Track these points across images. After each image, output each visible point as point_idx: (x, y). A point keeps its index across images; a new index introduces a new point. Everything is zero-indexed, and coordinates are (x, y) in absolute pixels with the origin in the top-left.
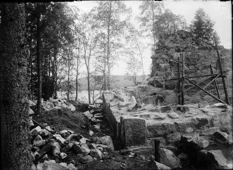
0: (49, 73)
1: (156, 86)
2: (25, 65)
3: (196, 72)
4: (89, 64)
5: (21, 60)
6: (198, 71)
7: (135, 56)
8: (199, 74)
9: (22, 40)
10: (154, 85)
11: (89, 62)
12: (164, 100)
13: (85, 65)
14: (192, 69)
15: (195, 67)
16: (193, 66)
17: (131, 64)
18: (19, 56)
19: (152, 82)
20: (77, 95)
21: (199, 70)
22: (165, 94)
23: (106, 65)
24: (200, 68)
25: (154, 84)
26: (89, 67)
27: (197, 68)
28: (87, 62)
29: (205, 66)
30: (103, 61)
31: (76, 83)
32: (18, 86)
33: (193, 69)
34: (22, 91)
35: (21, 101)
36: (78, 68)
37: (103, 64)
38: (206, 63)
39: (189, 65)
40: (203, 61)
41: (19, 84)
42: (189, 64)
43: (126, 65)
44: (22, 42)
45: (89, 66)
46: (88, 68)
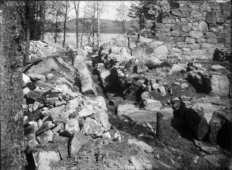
0: (37, 16)
1: (146, 37)
2: (20, 66)
3: (187, 24)
4: (78, 9)
5: (15, 59)
6: (190, 24)
7: (184, 49)
8: (190, 26)
9: (16, 30)
10: (144, 35)
11: (78, 7)
12: (154, 51)
13: (74, 9)
14: (183, 21)
15: (186, 19)
16: (184, 18)
17: (121, 11)
18: (12, 54)
19: (143, 33)
20: (64, 40)
21: (190, 22)
22: (155, 45)
23: (95, 11)
24: (191, 21)
25: (145, 34)
26: (78, 12)
27: (188, 20)
28: (77, 7)
29: (196, 20)
30: (92, 7)
31: (64, 27)
32: (10, 98)
33: (184, 22)
34: (16, 103)
35: (14, 119)
36: (67, 12)
37: (92, 10)
38: (198, 16)
39: (181, 18)
40: (195, 13)
41: (10, 95)
42: (181, 17)
43: (116, 12)
44: (16, 33)
45: (78, 11)
46: (77, 13)
